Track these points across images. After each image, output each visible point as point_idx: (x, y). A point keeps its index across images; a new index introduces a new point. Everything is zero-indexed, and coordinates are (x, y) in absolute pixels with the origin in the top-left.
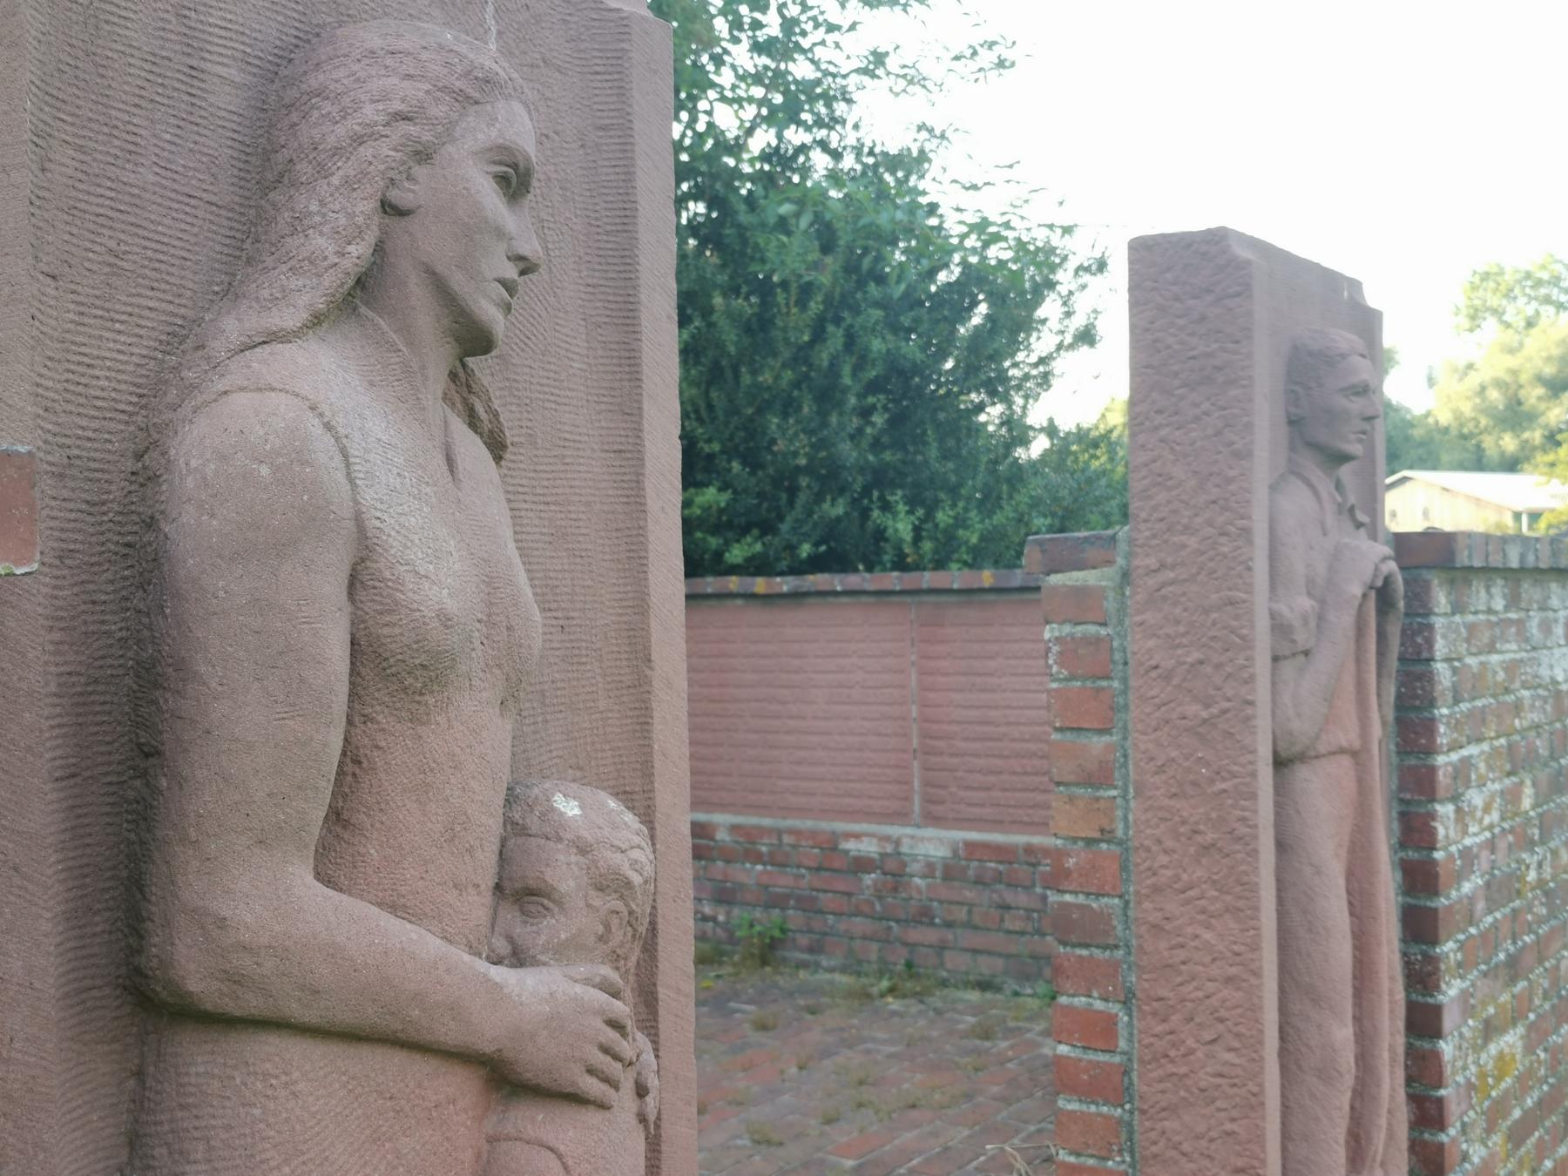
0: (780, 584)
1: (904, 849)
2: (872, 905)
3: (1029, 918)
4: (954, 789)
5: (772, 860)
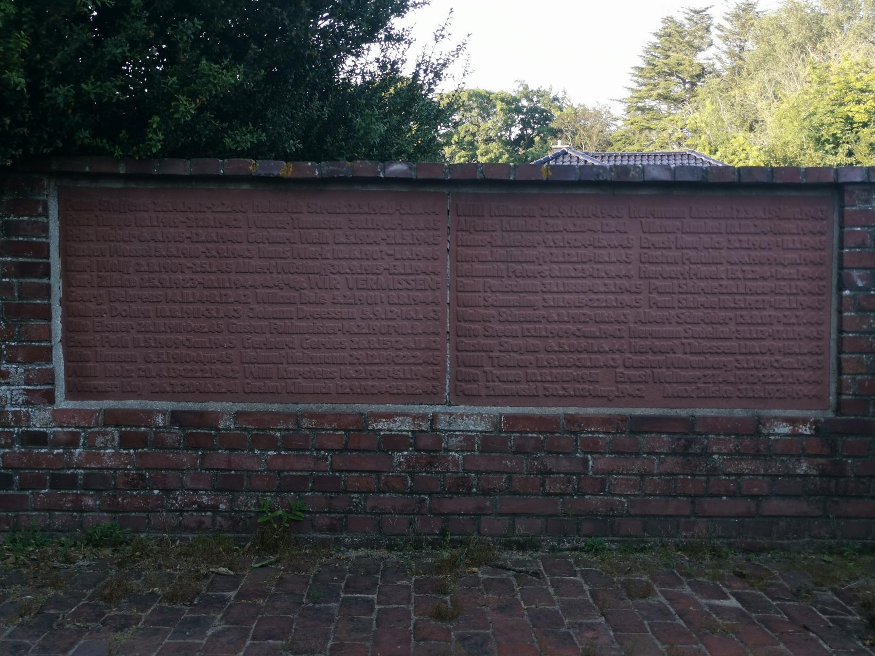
0: (312, 169)
1: (441, 426)
2: (404, 479)
3: (569, 481)
4: (488, 369)
5: (287, 444)
